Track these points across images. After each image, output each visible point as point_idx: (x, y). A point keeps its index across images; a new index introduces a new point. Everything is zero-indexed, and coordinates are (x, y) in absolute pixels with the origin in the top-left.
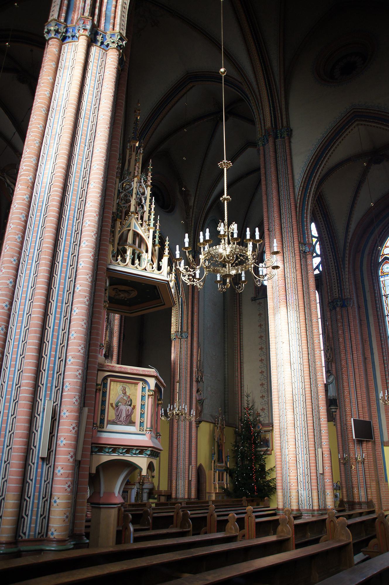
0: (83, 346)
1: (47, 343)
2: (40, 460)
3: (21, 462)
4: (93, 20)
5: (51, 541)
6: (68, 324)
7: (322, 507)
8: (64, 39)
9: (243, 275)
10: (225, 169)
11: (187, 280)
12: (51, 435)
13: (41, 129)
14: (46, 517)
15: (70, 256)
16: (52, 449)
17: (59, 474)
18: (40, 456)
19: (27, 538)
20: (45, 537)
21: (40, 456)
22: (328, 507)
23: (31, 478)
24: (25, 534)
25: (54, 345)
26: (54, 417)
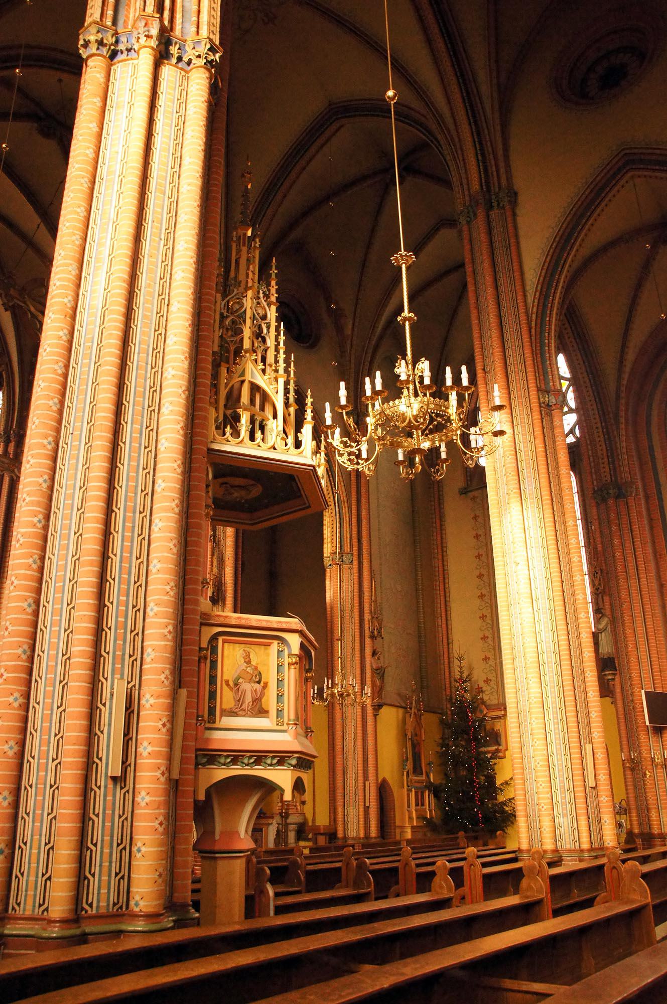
0: (172, 584)
1: (112, 582)
2: (110, 781)
3: (78, 786)
4: (161, 19)
5: (135, 916)
6: (146, 547)
7: (596, 845)
8: (113, 55)
9: (443, 449)
10: (404, 267)
11: (346, 461)
12: (126, 738)
13: (82, 215)
14: (124, 877)
15: (144, 430)
16: (128, 763)
17: (143, 804)
18: (109, 774)
19: (94, 912)
20: (124, 909)
21: (109, 774)
22: (606, 845)
23: (97, 812)
24: (91, 905)
25: (135, 447)
26: (130, 706)
